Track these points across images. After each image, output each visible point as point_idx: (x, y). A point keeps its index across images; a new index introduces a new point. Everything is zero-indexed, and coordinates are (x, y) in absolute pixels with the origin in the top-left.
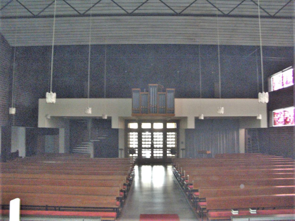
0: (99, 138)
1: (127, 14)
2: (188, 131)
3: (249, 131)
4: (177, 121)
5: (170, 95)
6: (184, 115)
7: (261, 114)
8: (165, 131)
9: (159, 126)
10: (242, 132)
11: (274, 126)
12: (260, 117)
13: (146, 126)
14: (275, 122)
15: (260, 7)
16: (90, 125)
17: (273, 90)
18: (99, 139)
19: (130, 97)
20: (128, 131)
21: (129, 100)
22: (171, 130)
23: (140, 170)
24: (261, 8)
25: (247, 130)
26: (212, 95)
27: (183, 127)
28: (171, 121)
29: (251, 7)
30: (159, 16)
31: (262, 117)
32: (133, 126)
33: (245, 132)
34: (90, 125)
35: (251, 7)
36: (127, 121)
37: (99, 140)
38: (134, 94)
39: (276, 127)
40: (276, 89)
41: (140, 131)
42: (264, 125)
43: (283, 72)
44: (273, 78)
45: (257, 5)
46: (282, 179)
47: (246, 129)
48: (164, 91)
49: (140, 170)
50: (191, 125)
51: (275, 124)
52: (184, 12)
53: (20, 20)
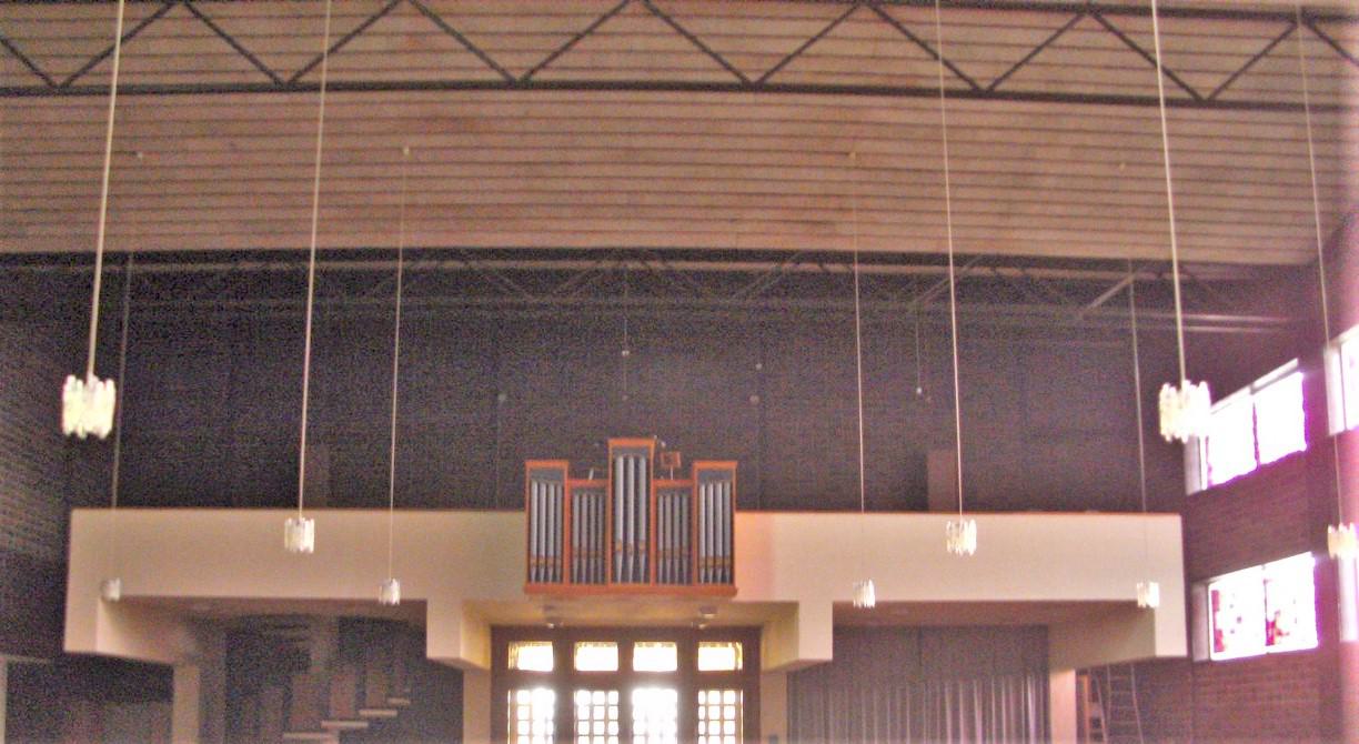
0: (394, 701)
1: (974, 90)
2: (804, 676)
3: (1099, 682)
4: (748, 636)
5: (712, 497)
6: (781, 595)
7: (1156, 581)
8: (690, 680)
9: (657, 657)
10: (1064, 686)
11: (1216, 657)
12: (1149, 596)
13: (595, 657)
14: (1218, 635)
15: (1154, 62)
16: (320, 649)
17: (1209, 482)
18: (369, 719)
19: (515, 500)
20: (505, 679)
21: (518, 518)
22: (719, 680)
23: (737, 663)
24: (1147, 55)
25: (1085, 680)
26: (914, 498)
27: (774, 657)
28: (719, 634)
29: (1104, 58)
30: (404, 92)
31: (1160, 595)
32: (534, 657)
33: (1079, 684)
34: (320, 649)
35: (1104, 58)
36: (503, 636)
37: (393, 713)
38: (538, 493)
39: (1224, 664)
40: (1220, 477)
41: (566, 679)
42: (1169, 642)
43: (1253, 392)
44: (1215, 594)
45: (1167, 73)
46: (1211, 313)
47: (1080, 673)
48: (685, 472)
49: (737, 663)
50: (815, 643)
51: (1219, 646)
52: (776, 79)
53: (197, 99)
